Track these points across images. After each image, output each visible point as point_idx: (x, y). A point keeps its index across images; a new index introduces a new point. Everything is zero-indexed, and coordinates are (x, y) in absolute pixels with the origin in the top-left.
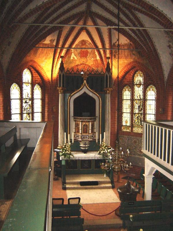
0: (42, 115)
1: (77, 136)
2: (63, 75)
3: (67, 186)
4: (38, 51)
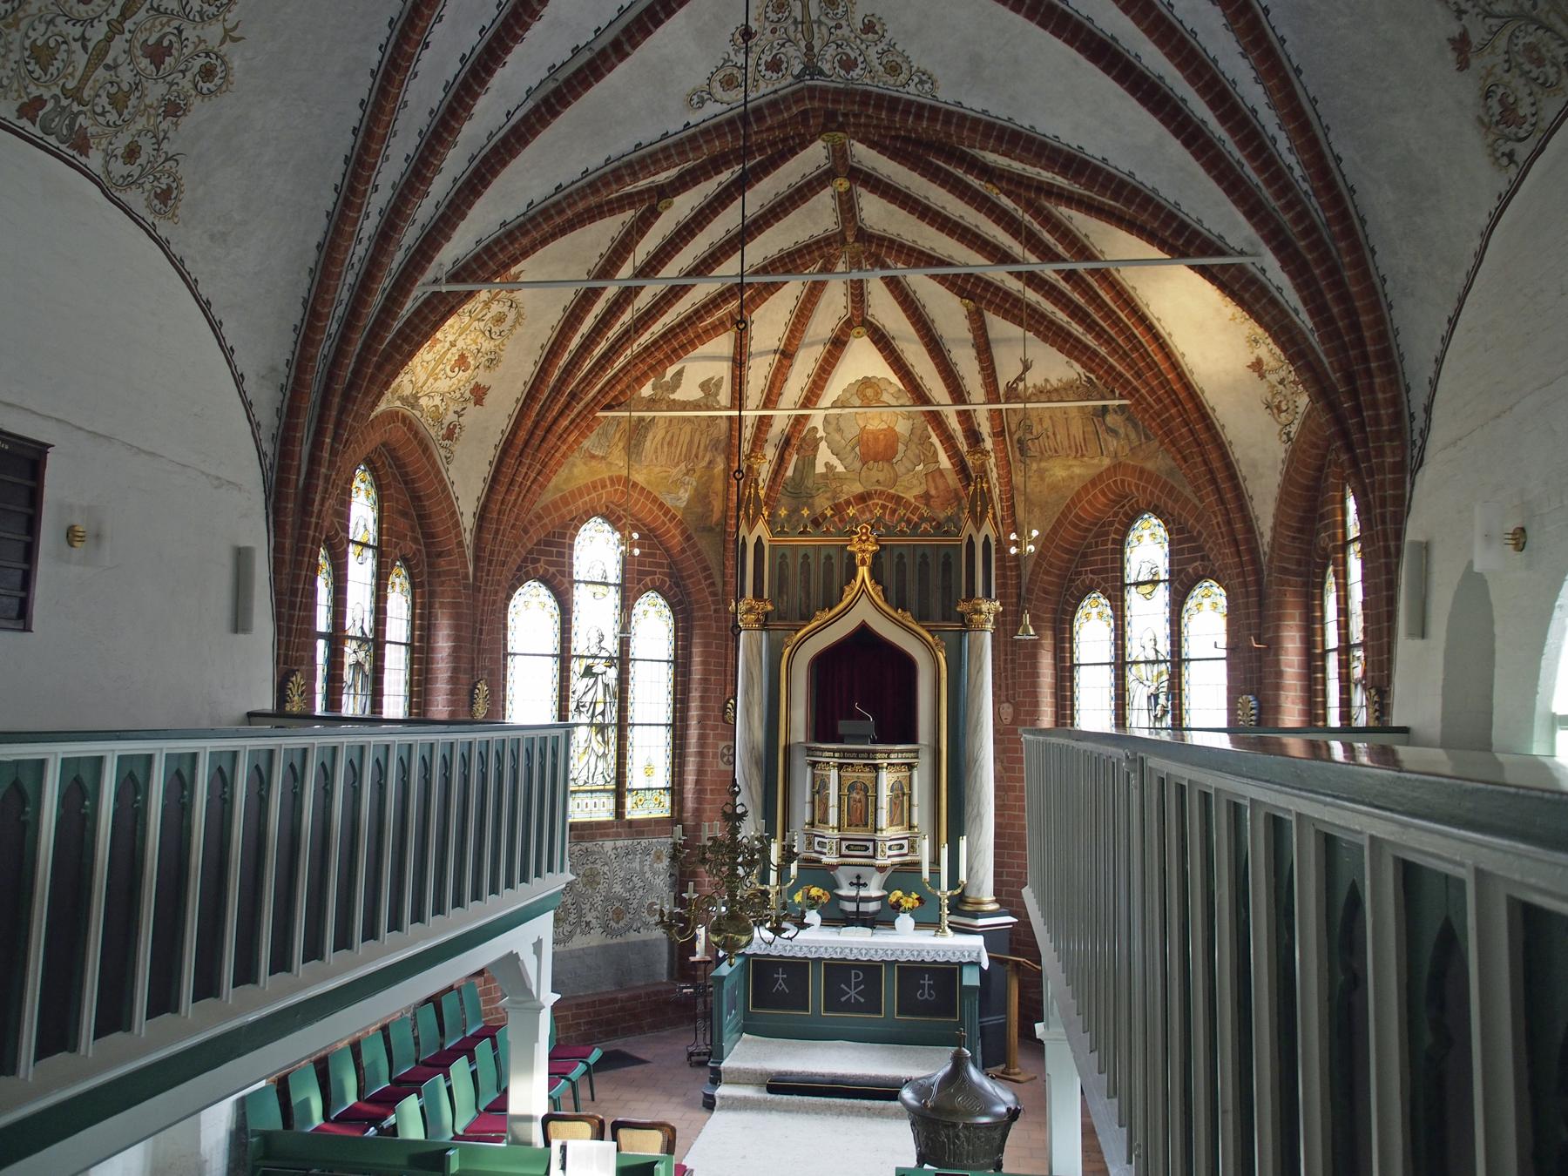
0: (674, 737)
1: (848, 847)
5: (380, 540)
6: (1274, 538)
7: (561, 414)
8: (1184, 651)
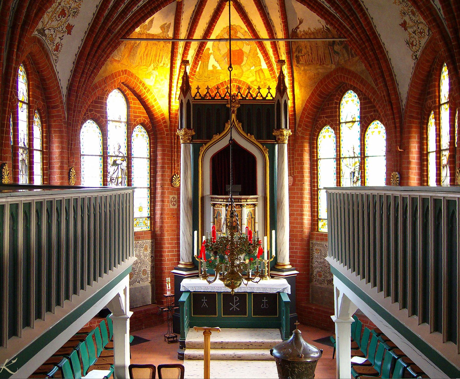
2: (188, 104)
3: (187, 352)
4: (138, 52)
5: (29, 100)
6: (407, 103)
7: (104, 39)
8: (366, 153)
